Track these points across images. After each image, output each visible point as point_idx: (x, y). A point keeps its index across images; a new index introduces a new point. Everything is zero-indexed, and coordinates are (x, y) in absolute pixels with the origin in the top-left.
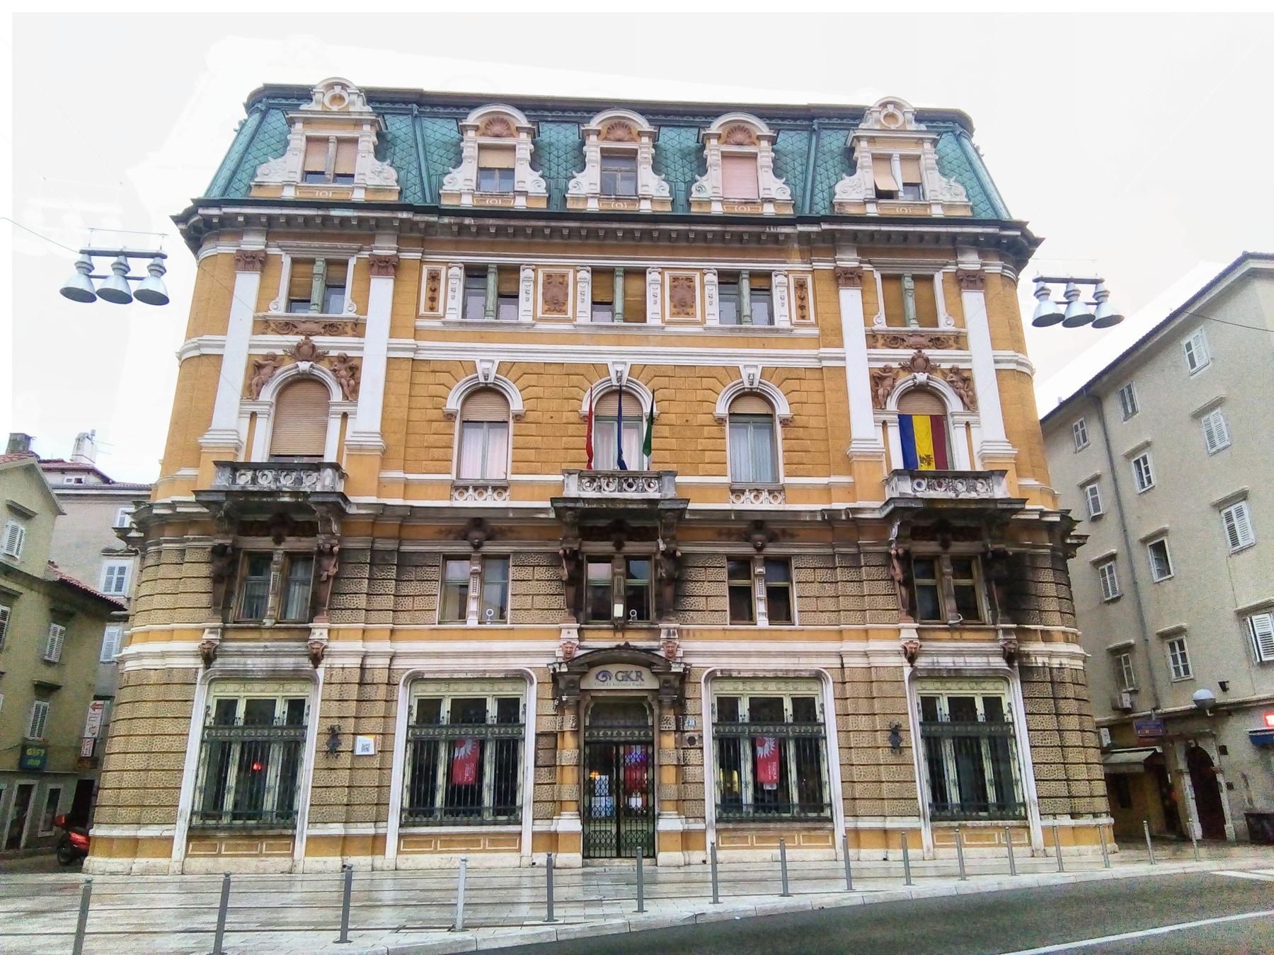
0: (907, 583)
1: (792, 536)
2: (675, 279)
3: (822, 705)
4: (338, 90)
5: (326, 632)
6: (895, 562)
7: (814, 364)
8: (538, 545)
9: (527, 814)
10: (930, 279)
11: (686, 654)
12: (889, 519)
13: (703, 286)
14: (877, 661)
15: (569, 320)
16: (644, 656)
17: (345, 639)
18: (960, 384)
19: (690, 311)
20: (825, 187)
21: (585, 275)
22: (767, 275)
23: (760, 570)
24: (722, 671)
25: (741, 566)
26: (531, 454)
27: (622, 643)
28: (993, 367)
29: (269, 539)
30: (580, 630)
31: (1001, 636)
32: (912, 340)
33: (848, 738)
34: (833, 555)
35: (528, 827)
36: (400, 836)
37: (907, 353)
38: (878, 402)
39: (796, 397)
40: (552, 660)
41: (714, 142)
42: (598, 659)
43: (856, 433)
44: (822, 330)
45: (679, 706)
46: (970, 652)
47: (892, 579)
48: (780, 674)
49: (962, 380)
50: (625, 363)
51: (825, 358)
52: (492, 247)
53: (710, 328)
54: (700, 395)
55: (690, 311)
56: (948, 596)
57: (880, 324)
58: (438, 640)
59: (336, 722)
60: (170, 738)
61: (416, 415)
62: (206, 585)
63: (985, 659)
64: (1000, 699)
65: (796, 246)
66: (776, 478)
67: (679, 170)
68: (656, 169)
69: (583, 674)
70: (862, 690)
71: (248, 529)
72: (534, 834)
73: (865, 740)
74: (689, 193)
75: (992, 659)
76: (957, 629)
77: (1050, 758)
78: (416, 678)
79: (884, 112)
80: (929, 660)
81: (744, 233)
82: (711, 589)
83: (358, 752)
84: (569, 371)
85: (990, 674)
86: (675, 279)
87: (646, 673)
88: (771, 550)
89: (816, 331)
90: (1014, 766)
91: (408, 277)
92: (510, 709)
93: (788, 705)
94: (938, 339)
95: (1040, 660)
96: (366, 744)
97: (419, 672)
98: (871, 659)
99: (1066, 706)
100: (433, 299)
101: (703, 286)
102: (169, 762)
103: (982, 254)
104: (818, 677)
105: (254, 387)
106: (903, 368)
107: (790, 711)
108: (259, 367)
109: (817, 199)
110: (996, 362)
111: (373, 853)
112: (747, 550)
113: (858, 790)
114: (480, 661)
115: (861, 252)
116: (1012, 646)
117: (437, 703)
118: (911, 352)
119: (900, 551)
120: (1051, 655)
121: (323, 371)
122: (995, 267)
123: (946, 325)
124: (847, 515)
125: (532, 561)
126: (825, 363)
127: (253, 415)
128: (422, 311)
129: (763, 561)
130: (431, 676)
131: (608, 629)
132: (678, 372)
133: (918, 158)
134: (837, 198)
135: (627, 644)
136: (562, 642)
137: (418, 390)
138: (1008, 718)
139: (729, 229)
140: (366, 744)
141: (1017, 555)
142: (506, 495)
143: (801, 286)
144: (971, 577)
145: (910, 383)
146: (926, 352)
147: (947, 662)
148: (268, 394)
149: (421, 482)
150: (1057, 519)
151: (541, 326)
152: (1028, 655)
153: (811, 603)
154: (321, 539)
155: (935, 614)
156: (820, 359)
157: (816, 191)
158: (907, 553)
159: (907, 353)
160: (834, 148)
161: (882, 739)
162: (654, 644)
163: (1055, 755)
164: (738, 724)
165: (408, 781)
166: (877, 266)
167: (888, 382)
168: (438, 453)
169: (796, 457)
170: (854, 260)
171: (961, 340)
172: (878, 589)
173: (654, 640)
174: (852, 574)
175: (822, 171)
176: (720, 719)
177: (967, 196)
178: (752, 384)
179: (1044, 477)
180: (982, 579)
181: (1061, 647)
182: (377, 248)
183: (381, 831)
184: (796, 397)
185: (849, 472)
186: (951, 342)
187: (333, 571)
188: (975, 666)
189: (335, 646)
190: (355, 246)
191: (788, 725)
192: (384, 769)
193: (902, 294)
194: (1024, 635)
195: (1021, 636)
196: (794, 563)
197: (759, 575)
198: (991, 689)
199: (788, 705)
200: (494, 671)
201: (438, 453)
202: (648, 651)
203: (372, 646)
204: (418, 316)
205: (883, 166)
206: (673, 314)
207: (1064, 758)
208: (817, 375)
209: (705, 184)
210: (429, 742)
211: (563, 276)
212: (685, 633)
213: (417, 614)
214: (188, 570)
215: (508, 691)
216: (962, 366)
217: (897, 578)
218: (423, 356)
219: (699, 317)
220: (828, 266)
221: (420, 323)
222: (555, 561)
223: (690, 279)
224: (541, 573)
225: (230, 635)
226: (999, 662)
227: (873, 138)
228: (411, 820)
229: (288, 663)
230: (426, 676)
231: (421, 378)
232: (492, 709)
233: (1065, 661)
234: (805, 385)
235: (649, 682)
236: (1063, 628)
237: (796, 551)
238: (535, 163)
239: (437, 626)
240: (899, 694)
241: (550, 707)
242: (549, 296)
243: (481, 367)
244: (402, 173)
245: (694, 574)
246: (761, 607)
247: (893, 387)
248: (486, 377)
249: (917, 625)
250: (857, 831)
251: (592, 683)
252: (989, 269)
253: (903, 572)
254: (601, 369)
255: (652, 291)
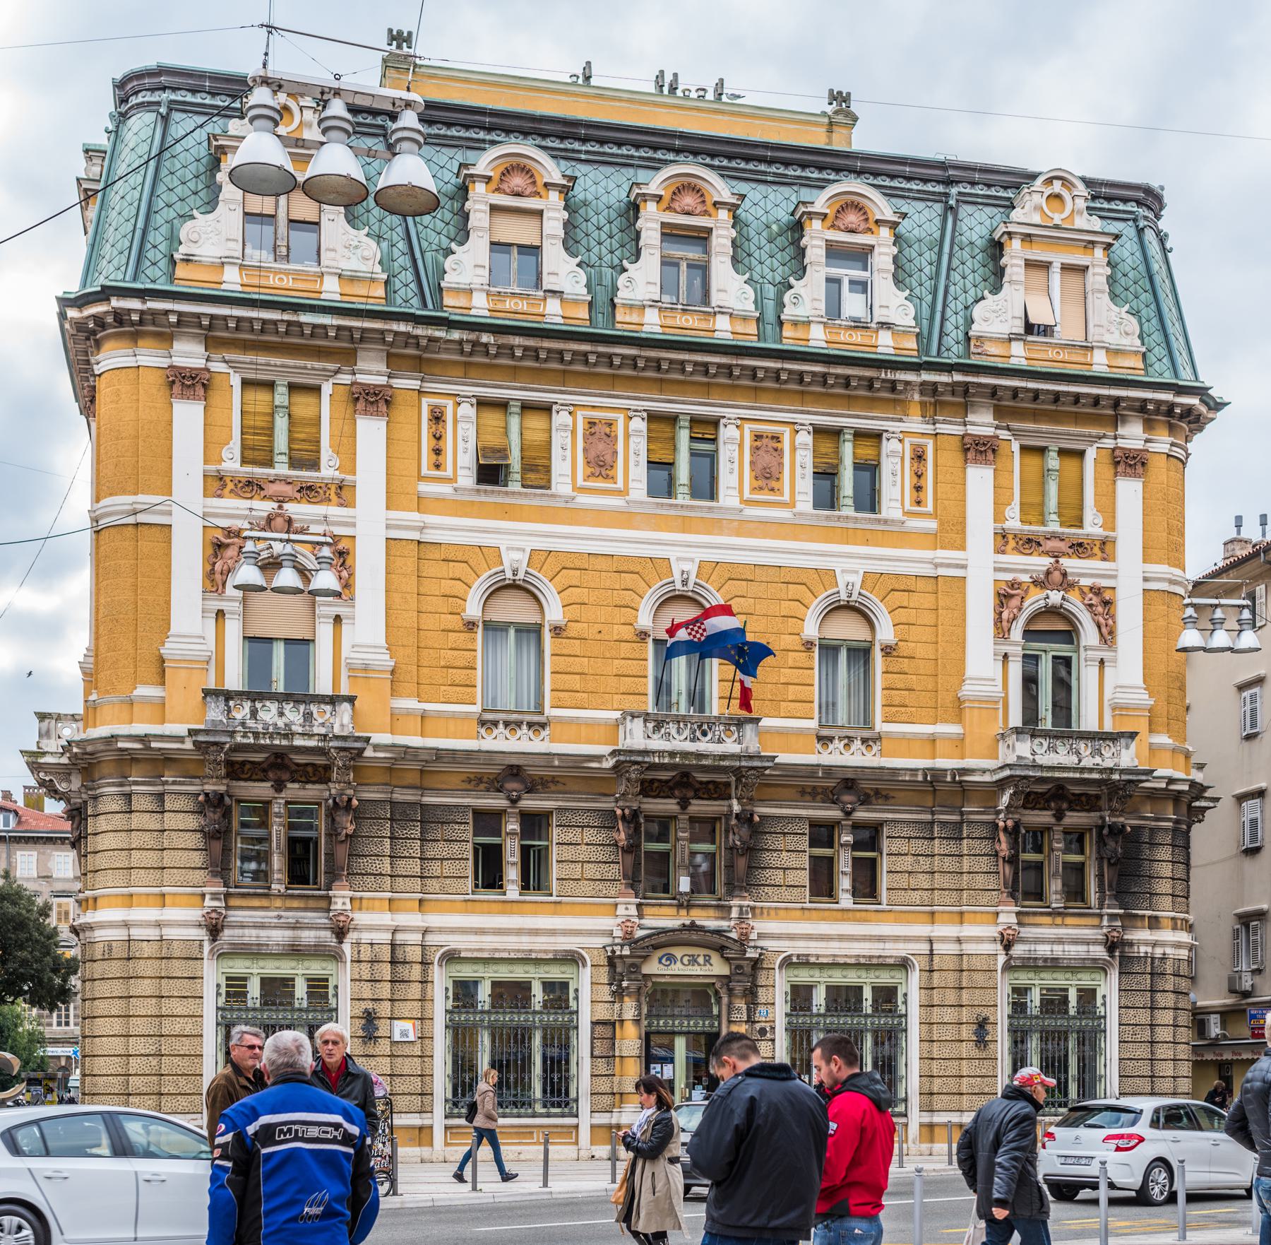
0: (1012, 860)
1: (887, 797)
2: (758, 437)
3: (577, 990)
4: (1057, 187)
5: (348, 901)
6: (1002, 836)
7: (928, 570)
8: (586, 801)
9: (584, 1106)
10: (1081, 454)
11: (761, 936)
12: (1001, 784)
13: (794, 449)
14: (969, 948)
15: (619, 493)
16: (716, 939)
17: (371, 909)
18: (1100, 609)
19: (611, 473)
20: (960, 307)
21: (639, 425)
22: (715, 423)
23: (847, 838)
24: (798, 956)
25: (822, 834)
26: (575, 682)
27: (688, 922)
28: (1141, 585)
29: (269, 784)
30: (639, 906)
31: (1105, 923)
32: (1050, 545)
33: (930, 1031)
34: (932, 823)
35: (585, 1120)
36: (447, 1128)
37: (1041, 563)
38: (1001, 629)
39: (902, 615)
40: (608, 940)
41: (817, 224)
42: (661, 941)
43: (971, 671)
44: (941, 524)
45: (751, 995)
46: (1068, 937)
47: (616, 845)
48: (862, 961)
49: (1103, 602)
50: (692, 560)
51: (942, 565)
52: (514, 373)
53: (801, 514)
54: (787, 607)
55: (774, 484)
56: (1055, 875)
57: (1014, 523)
58: (512, 913)
59: (370, 1005)
60: (182, 1020)
61: (429, 622)
62: (195, 840)
63: (1084, 948)
64: (567, 984)
65: (917, 397)
66: (868, 722)
67: (771, 265)
68: (898, 282)
69: (646, 958)
70: (951, 979)
71: (236, 770)
72: (592, 1126)
73: (950, 1032)
74: (780, 305)
75: (1092, 948)
76: (1060, 914)
77: (1138, 1054)
78: (451, 957)
79: (1048, 192)
80: (1026, 947)
81: (856, 378)
82: (790, 860)
83: (397, 1038)
84: (624, 567)
85: (1088, 964)
86: (758, 437)
87: (715, 958)
88: (862, 815)
89: (932, 525)
90: (1100, 1061)
91: (403, 413)
92: (558, 993)
93: (867, 994)
94: (1080, 545)
95: (1143, 949)
96: (404, 1029)
97: (455, 950)
98: (964, 946)
99: (1162, 1000)
100: (438, 452)
101: (794, 449)
102: (185, 1046)
103: (1149, 425)
104: (903, 965)
105: (218, 577)
106: (1035, 583)
107: (870, 1002)
108: (219, 547)
109: (949, 327)
110: (1146, 579)
111: (420, 1145)
112: (834, 813)
113: (937, 1085)
114: (525, 939)
115: (999, 412)
116: (1115, 934)
117: (809, 989)
118: (1047, 561)
119: (1010, 823)
120: (1155, 944)
121: (1076, 605)
122: (1162, 443)
123: (1092, 526)
124: (925, 776)
125: (579, 819)
126: (941, 571)
127: (220, 614)
128: (425, 471)
129: (852, 826)
130: (469, 955)
131: (671, 905)
132: (602, 564)
133: (1084, 269)
134: (975, 330)
135: (693, 923)
136: (619, 920)
137: (429, 587)
138: (1101, 1010)
139: (832, 371)
140: (404, 1029)
141: (1136, 829)
142: (544, 733)
143: (919, 457)
144: (1082, 852)
145: (1042, 603)
146: (1065, 562)
147: (1044, 950)
148: (1017, 633)
149: (440, 715)
150: (1186, 788)
151: (585, 500)
152: (1131, 944)
153: (903, 881)
154: (334, 788)
155: (1038, 894)
156: (936, 566)
157: (949, 313)
158: (1017, 825)
159: (1041, 563)
160: (974, 237)
161: (967, 1032)
162: (724, 924)
163: (1143, 1051)
164: (812, 1016)
165: (449, 1071)
166: (1016, 434)
167: (1015, 602)
168: (459, 675)
169: (897, 696)
170: (379, 374)
171: (1108, 547)
172: (977, 865)
173: (723, 918)
174: (951, 847)
175: (958, 277)
176: (793, 1008)
177: (1141, 337)
178: (850, 595)
179: (1181, 735)
180: (1094, 856)
181: (1167, 935)
182: (362, 372)
183: (427, 1122)
184: (902, 615)
185: (959, 719)
186: (1096, 550)
187: (351, 828)
188: (1073, 955)
189: (361, 918)
190: (332, 366)
191: (867, 1016)
192: (425, 1056)
193: (1045, 473)
194: (1130, 920)
195: (1127, 923)
196: (886, 831)
197: (513, 833)
198: (1086, 980)
199: (867, 994)
200: (540, 951)
201: (459, 675)
202: (718, 932)
203: (403, 919)
204: (421, 478)
205: (1038, 275)
206: (753, 489)
207: (1152, 1053)
208: (930, 586)
209: (802, 292)
210: (560, 1029)
211: (776, 438)
212: (758, 911)
213: (448, 881)
214: (171, 821)
215: (555, 973)
216: (1104, 583)
217: (1002, 854)
218: (429, 536)
219: (620, 485)
220: (958, 430)
221: (424, 488)
222: (608, 820)
223: (776, 438)
224: (590, 835)
225: (233, 902)
226: (1099, 952)
227: (1029, 235)
228: (456, 1111)
229: (308, 937)
230: (463, 955)
231: (431, 569)
232: (301, 990)
233: (1169, 951)
234: (915, 600)
235: (718, 967)
236: (1172, 914)
237: (890, 816)
238: (570, 243)
239: (470, 897)
240: (991, 984)
241: (605, 993)
242: (592, 454)
243: (842, 580)
244: (385, 245)
245: (771, 841)
246: (845, 883)
247: (1020, 609)
248: (515, 572)
249: (351, 893)
250: (931, 1126)
251: (653, 967)
252: (1152, 447)
253: (629, 837)
254: (661, 565)
255: (560, 440)
